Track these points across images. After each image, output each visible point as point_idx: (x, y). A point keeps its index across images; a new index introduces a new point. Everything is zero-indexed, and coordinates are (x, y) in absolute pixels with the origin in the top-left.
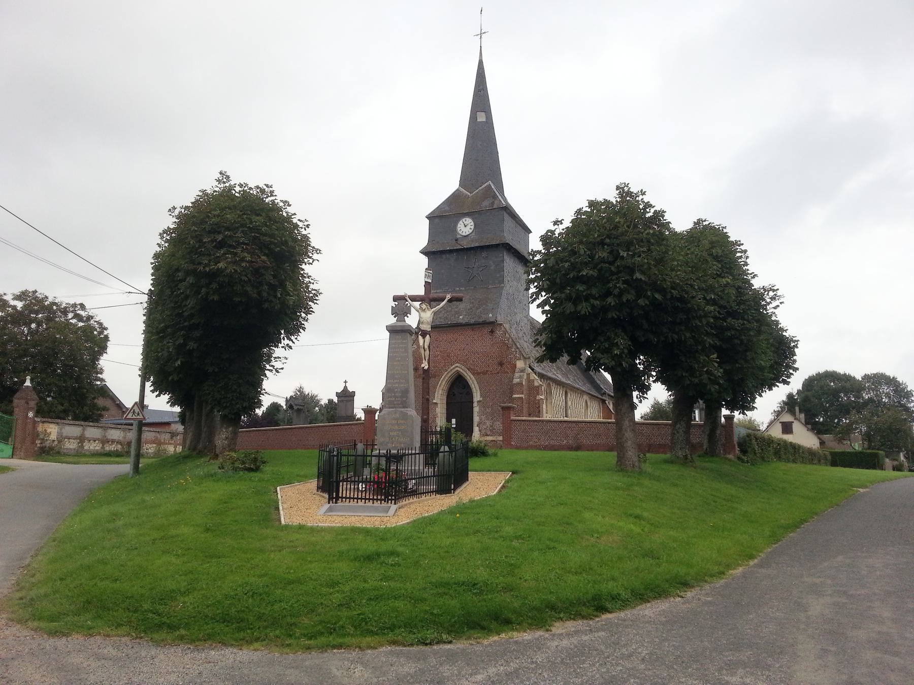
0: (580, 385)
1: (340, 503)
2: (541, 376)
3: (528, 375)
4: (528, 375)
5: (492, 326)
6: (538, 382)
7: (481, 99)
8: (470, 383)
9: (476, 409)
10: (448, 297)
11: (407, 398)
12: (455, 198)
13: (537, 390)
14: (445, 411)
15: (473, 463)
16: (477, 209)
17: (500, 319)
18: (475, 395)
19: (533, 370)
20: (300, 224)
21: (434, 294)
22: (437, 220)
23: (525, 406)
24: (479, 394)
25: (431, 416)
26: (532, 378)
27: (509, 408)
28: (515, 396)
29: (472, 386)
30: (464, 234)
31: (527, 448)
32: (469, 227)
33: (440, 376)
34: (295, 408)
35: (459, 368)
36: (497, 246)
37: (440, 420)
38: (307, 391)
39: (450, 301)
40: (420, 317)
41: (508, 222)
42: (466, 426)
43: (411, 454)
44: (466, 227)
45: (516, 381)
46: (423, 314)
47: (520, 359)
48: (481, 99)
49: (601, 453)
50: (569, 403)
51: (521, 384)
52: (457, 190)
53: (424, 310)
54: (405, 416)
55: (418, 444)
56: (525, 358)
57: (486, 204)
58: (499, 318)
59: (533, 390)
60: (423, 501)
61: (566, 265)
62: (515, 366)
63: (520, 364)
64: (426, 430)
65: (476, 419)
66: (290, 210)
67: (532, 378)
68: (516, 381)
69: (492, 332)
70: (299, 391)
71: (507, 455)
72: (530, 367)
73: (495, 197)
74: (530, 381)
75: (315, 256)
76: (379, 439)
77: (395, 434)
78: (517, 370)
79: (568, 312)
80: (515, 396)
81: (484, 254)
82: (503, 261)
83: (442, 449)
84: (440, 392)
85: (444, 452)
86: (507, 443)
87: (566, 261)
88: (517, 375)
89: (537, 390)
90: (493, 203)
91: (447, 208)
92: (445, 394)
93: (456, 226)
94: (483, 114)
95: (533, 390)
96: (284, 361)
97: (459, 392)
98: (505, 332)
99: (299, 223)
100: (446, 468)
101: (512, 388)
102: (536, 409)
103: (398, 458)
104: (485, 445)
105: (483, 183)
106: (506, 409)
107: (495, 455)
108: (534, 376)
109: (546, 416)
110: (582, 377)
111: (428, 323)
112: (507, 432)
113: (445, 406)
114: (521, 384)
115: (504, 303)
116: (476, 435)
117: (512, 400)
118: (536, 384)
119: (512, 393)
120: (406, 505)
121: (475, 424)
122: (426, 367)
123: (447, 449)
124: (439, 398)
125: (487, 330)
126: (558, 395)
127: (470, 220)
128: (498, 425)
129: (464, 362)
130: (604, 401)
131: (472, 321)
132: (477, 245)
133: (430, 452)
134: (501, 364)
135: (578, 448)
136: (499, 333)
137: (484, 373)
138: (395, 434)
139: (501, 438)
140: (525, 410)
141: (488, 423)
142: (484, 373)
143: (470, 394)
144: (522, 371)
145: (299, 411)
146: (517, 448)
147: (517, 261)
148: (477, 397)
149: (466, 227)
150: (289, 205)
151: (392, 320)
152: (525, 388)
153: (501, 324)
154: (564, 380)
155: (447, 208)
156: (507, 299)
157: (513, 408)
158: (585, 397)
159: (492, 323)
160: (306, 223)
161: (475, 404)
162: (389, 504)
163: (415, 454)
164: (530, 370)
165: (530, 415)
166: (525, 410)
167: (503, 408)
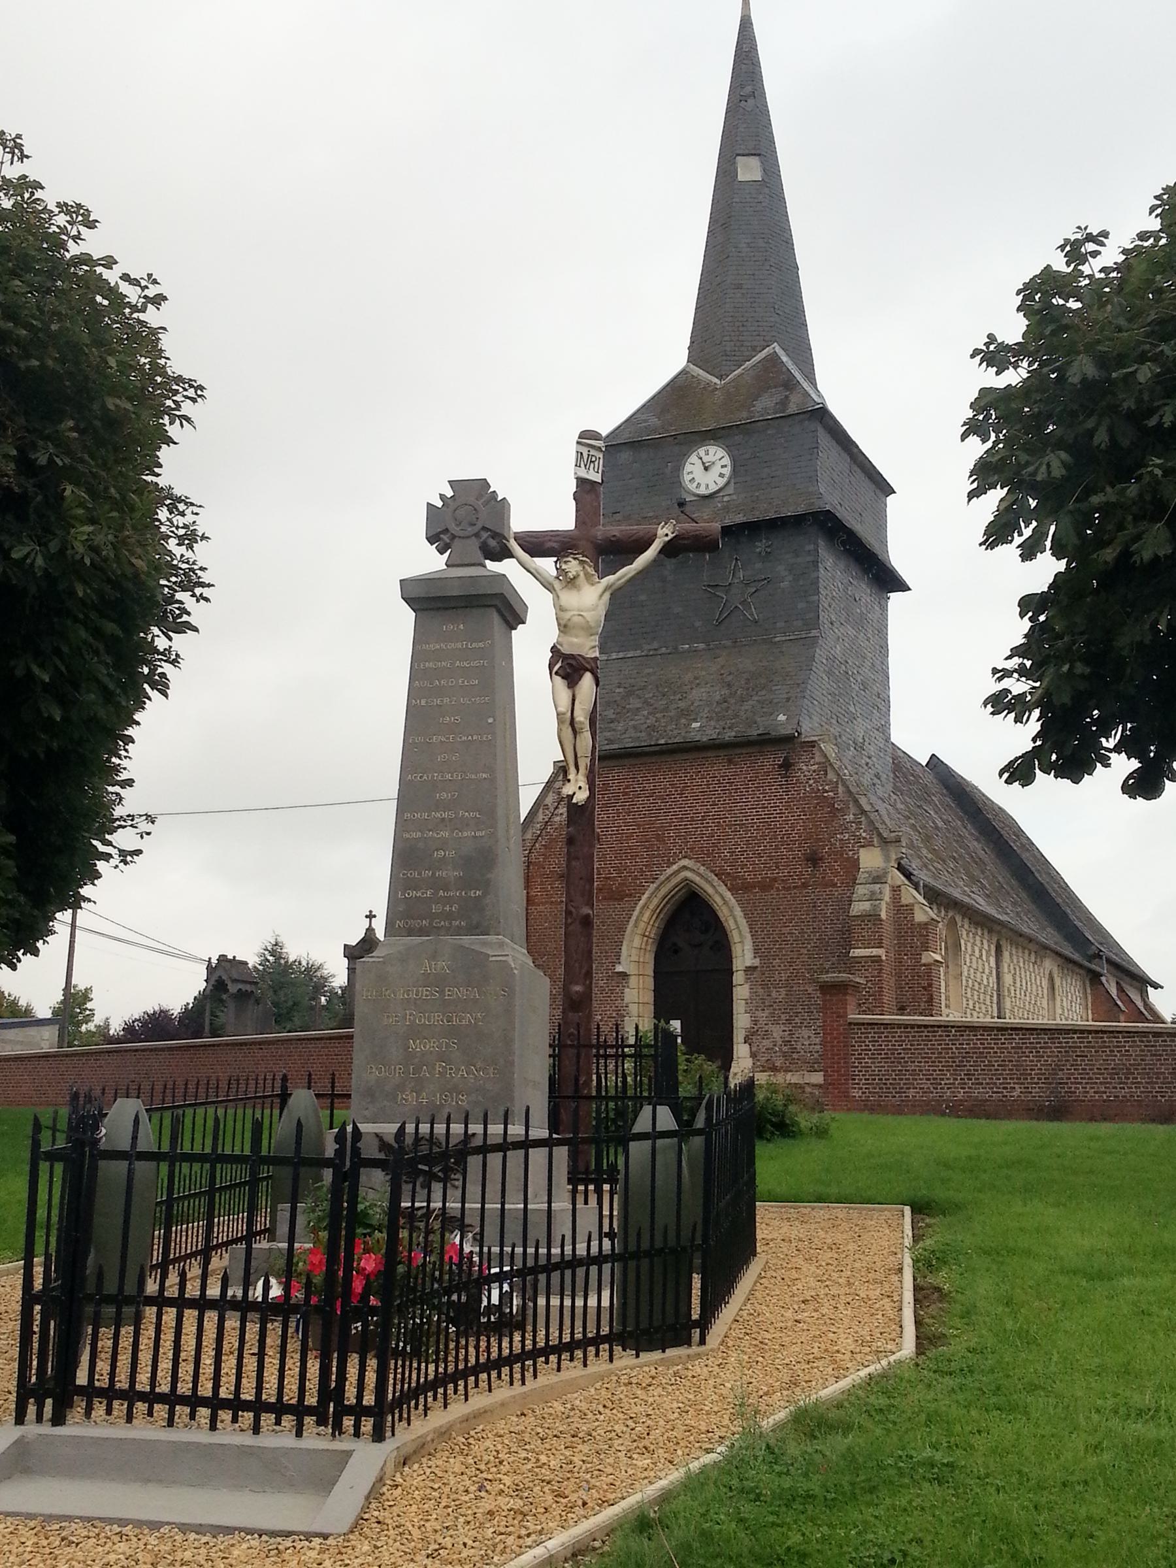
0: (1030, 926)
1: (75, 1427)
2: (934, 896)
3: (896, 890)
4: (896, 890)
5: (785, 748)
6: (923, 913)
7: (747, 122)
8: (723, 913)
9: (741, 992)
10: (665, 533)
11: (486, 886)
12: (676, 393)
13: (921, 935)
14: (649, 997)
15: (772, 1163)
16: (742, 416)
17: (809, 729)
18: (737, 950)
19: (908, 875)
20: (132, 294)
21: (608, 529)
22: (625, 456)
23: (889, 983)
24: (748, 945)
25: (599, 979)
26: (905, 900)
27: (840, 989)
28: (856, 952)
29: (730, 924)
30: (702, 491)
31: (898, 1110)
32: (716, 470)
33: (635, 895)
34: (233, 988)
35: (688, 870)
36: (797, 521)
37: (635, 1008)
38: (294, 952)
39: (669, 550)
40: (560, 609)
41: (829, 455)
42: (715, 1040)
43: (504, 1147)
44: (707, 471)
45: (860, 907)
46: (570, 598)
47: (870, 844)
48: (747, 122)
49: (1137, 1126)
50: (1008, 979)
51: (873, 917)
52: (684, 372)
53: (571, 582)
54: (476, 970)
55: (538, 1102)
56: (885, 842)
57: (766, 404)
58: (806, 727)
59: (911, 937)
60: (547, 1395)
61: (1145, 373)
62: (855, 864)
63: (870, 859)
64: (576, 1041)
65: (741, 1021)
66: (92, 244)
67: (905, 900)
68: (860, 907)
69: (787, 765)
70: (272, 953)
71: (860, 1135)
72: (900, 868)
73: (790, 384)
74: (902, 911)
75: (187, 408)
76: (363, 1072)
77: (430, 1046)
78: (861, 877)
79: (1147, 555)
80: (856, 952)
81: (760, 546)
82: (815, 564)
83: (642, 1123)
84: (637, 941)
85: (654, 1135)
86: (836, 1091)
87: (1142, 358)
88: (861, 890)
89: (921, 935)
90: (784, 403)
91: (654, 421)
92: (651, 948)
93: (678, 469)
94: (754, 162)
95: (911, 937)
96: (144, 826)
97: (690, 937)
98: (826, 765)
99: (125, 288)
100: (666, 1216)
101: (848, 931)
102: (920, 989)
103: (442, 1161)
104: (789, 1100)
105: (756, 350)
106: (835, 990)
107: (821, 1133)
108: (911, 895)
109: (951, 1014)
110: (1032, 907)
111: (588, 630)
112: (836, 1057)
113: (650, 983)
114: (873, 917)
115: (820, 684)
116: (742, 1064)
117: (851, 965)
118: (920, 917)
119: (848, 944)
120: (444, 1434)
121: (739, 1036)
122: (581, 796)
123: (666, 1119)
124: (634, 957)
125: (770, 761)
126: (976, 951)
127: (721, 452)
128: (809, 1039)
129: (705, 856)
130: (1095, 978)
131: (729, 735)
132: (740, 519)
133: (587, 1128)
134: (813, 860)
135: (1058, 1111)
136: (805, 768)
137: (765, 886)
138: (430, 1046)
139: (818, 1078)
140: (889, 997)
141: (777, 1032)
142: (765, 886)
143: (722, 946)
144: (878, 879)
145: (242, 996)
146: (873, 1108)
147: (855, 570)
148: (744, 955)
149: (707, 471)
150: (91, 225)
151: (431, 562)
152: (888, 929)
153: (813, 744)
154: (991, 911)
155: (654, 421)
156: (829, 673)
157: (856, 987)
158: (1049, 964)
159: (789, 739)
160: (152, 292)
161: (738, 978)
162: (344, 1444)
163: (526, 1144)
164: (900, 878)
165: (902, 1010)
166: (889, 997)
167: (828, 989)
